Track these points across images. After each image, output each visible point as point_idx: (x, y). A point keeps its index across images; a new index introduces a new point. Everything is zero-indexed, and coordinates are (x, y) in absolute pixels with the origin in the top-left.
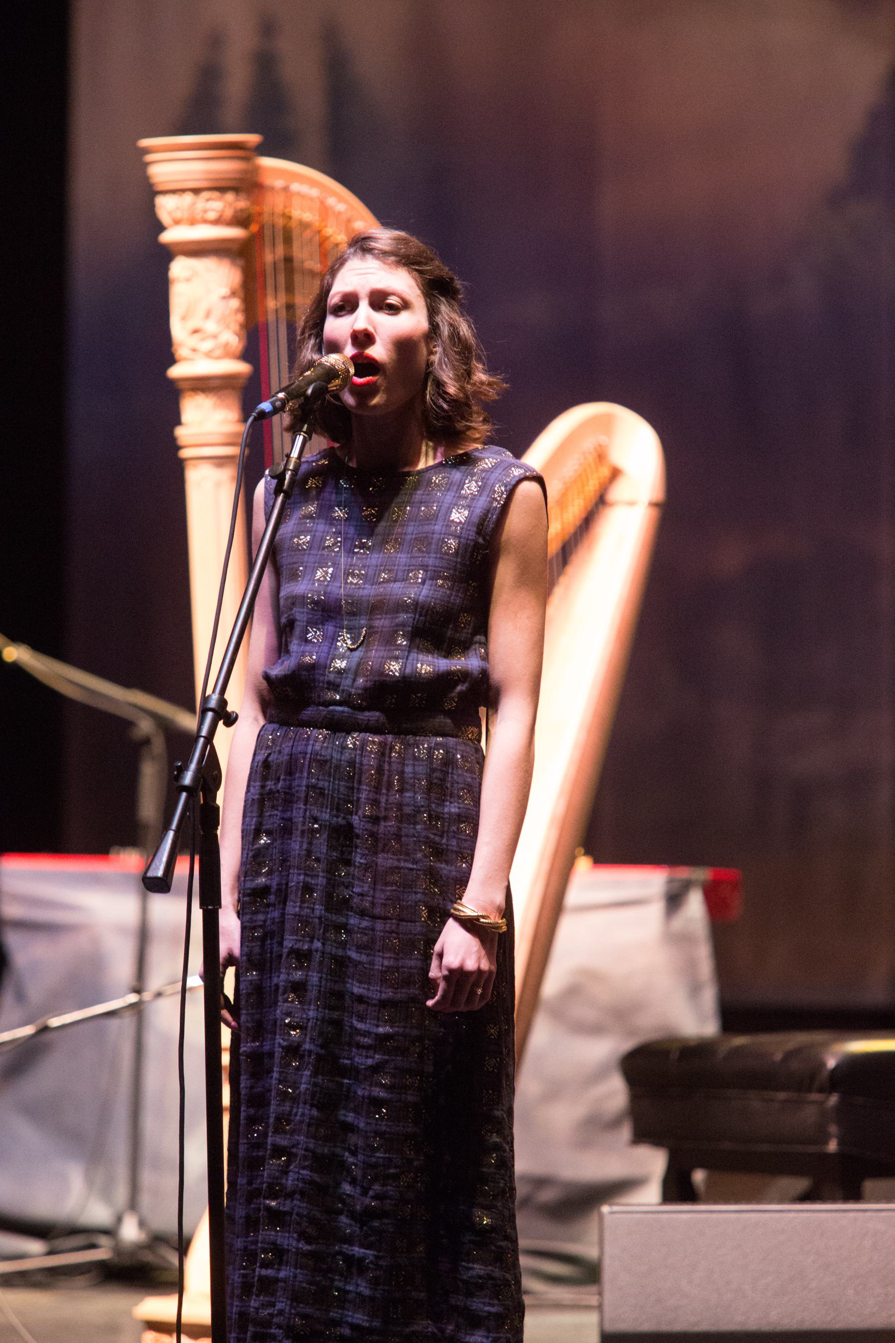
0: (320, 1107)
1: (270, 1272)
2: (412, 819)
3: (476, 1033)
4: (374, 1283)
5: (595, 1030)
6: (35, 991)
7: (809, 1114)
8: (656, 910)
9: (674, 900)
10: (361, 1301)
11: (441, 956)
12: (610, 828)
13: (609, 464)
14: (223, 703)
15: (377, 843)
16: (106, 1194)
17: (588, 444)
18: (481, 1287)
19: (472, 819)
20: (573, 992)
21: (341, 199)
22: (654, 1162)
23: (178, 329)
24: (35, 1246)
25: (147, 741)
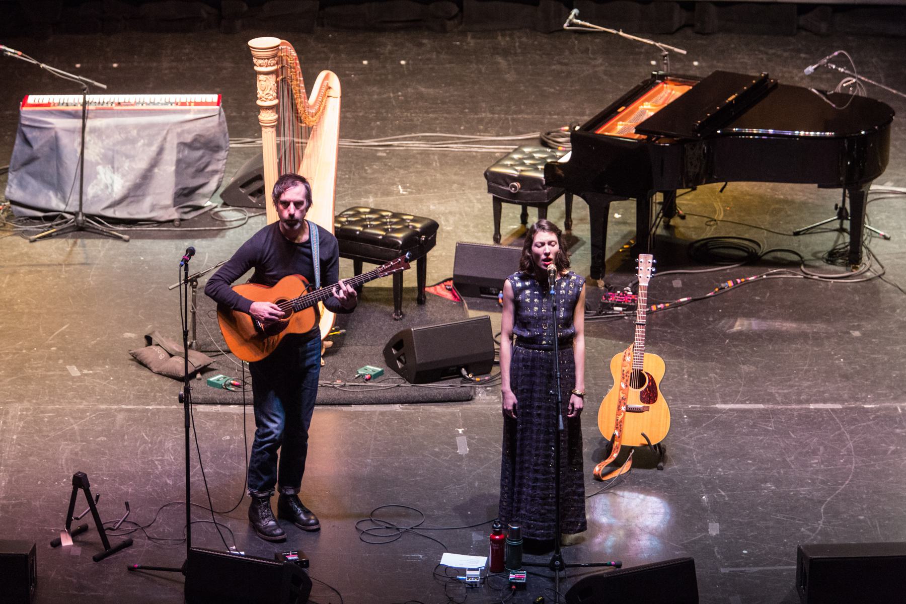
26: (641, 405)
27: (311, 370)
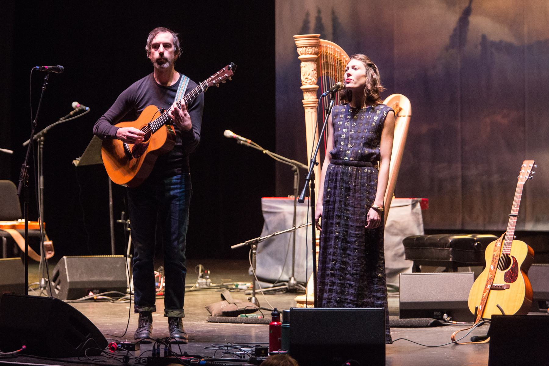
0: (343, 250)
1: (331, 287)
2: (364, 185)
3: (375, 235)
4: (355, 290)
5: (397, 235)
6: (270, 228)
7: (445, 252)
8: (410, 207)
9: (414, 205)
10: (352, 294)
11: (369, 216)
12: (401, 189)
13: (400, 107)
14: (315, 160)
15: (355, 191)
16: (287, 273)
17: (394, 103)
18: (380, 291)
19: (376, 185)
20: (391, 226)
21: (338, 48)
22: (410, 264)
23: (303, 78)
24: (271, 285)
25: (296, 171)
26: (503, 283)
27: (174, 202)
